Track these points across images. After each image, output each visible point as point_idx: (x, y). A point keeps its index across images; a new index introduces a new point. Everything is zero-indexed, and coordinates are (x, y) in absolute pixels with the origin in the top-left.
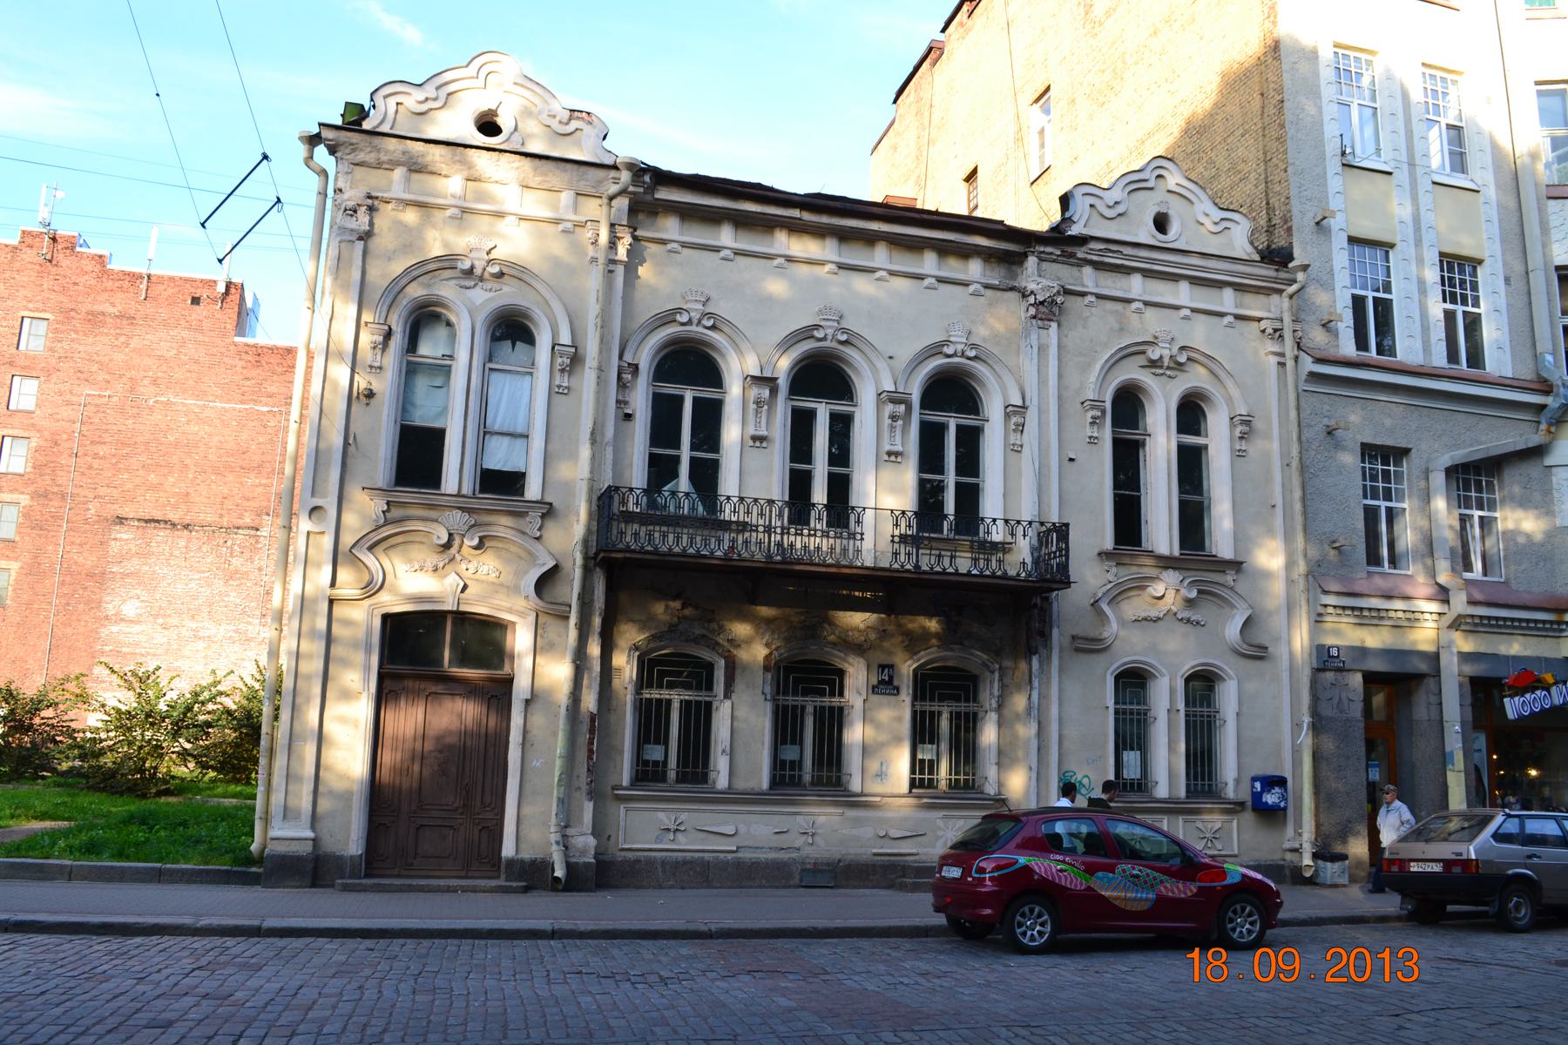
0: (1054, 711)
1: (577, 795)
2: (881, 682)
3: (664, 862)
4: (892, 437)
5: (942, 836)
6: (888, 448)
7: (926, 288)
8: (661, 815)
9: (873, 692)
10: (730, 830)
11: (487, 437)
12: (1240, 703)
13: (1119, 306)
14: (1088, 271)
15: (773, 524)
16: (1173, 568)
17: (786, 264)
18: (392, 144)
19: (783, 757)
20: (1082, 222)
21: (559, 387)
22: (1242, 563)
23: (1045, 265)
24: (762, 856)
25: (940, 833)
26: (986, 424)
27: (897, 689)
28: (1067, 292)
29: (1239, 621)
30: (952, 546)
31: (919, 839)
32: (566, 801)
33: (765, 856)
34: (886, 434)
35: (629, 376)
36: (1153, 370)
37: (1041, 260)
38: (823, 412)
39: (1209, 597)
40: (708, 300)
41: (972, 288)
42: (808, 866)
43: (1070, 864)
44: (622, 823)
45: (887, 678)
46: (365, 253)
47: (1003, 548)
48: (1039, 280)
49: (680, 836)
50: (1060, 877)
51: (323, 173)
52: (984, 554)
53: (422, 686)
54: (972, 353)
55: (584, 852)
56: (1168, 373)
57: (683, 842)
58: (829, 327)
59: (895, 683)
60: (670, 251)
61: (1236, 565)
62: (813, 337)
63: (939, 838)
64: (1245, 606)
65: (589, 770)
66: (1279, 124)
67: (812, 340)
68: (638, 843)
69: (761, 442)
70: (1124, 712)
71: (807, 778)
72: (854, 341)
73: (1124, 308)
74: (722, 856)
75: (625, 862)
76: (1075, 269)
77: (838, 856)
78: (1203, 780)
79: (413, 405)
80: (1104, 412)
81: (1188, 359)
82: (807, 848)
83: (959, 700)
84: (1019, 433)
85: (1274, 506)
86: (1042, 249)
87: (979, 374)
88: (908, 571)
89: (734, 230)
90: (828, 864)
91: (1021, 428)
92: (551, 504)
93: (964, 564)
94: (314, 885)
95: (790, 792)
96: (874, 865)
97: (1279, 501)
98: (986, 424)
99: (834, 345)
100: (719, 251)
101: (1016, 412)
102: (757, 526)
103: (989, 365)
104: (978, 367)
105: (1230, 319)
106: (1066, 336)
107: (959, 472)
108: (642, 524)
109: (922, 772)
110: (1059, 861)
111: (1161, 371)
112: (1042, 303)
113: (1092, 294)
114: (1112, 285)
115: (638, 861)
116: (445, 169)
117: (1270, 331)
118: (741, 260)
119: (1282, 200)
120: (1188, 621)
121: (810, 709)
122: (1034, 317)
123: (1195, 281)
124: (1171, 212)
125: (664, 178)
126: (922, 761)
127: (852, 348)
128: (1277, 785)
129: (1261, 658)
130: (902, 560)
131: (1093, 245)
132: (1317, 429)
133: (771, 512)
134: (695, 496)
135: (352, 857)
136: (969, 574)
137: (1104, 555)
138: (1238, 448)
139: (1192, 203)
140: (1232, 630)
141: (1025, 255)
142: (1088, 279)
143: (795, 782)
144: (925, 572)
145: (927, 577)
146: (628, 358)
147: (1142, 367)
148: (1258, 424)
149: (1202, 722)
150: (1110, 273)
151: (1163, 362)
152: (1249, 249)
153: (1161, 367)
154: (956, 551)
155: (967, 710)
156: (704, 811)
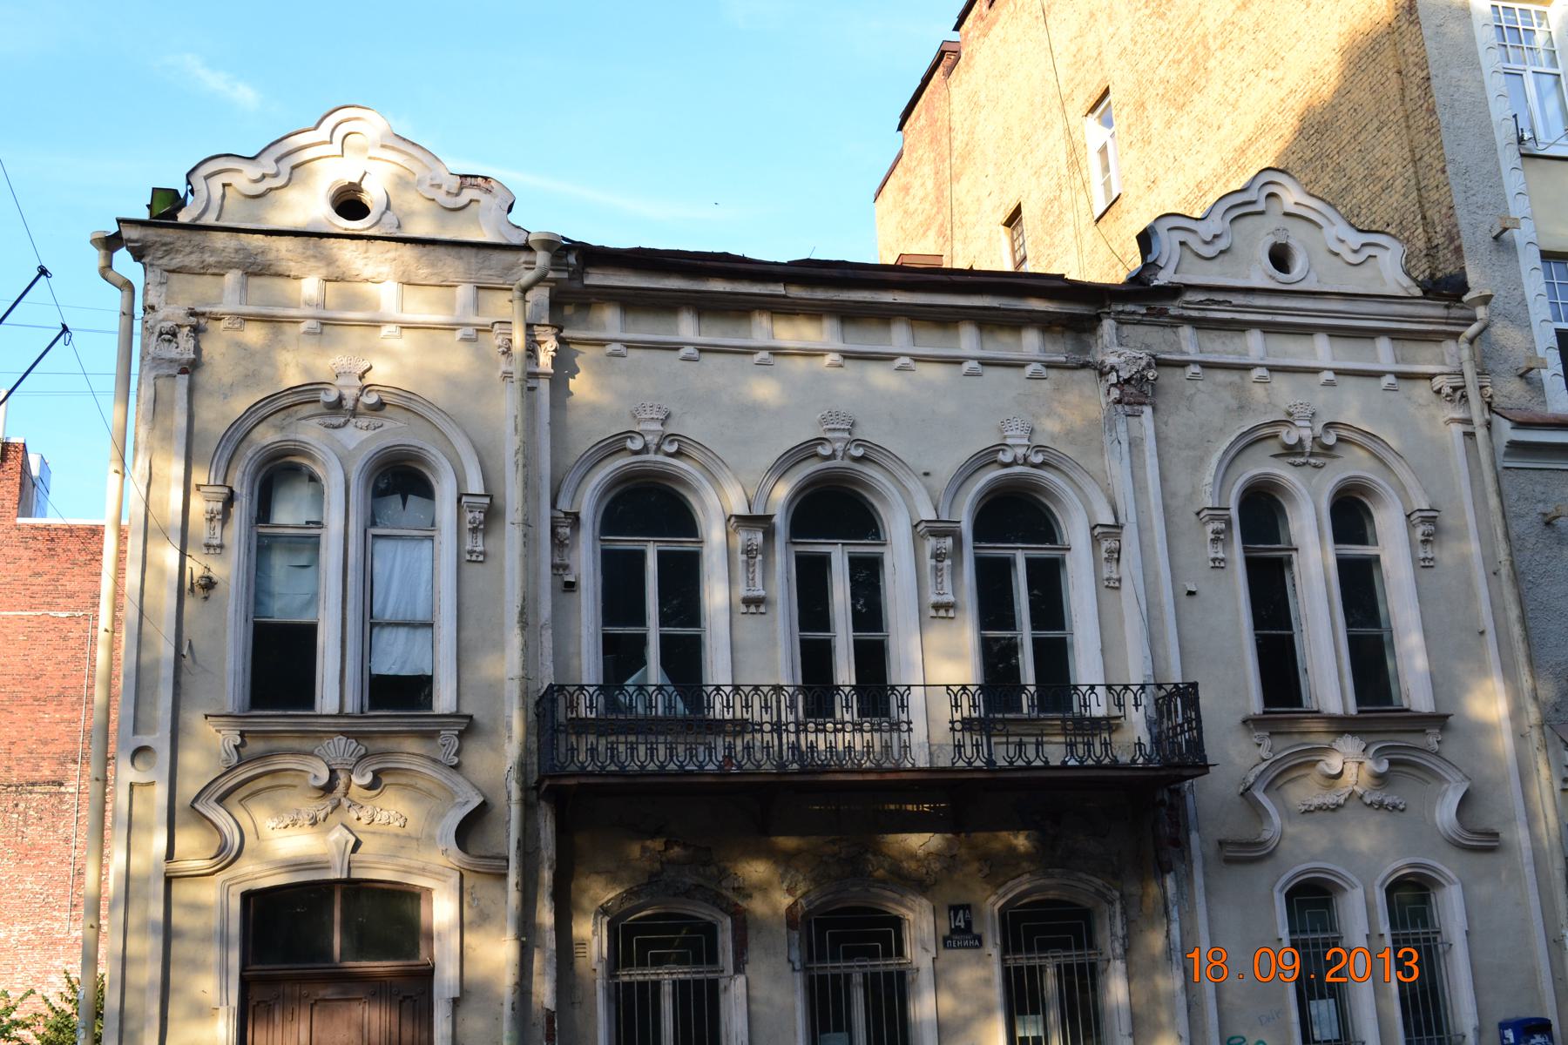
2: (955, 931)
4: (938, 584)
6: (933, 598)
7: (967, 375)
11: (375, 631)
12: (1469, 918)
13: (1234, 377)
14: (1186, 332)
17: (913, 364)
18: (220, 240)
21: (471, 552)
23: (1126, 330)
26: (1294, 554)
27: (979, 938)
28: (1161, 364)
34: (929, 580)
36: (1292, 460)
37: (1120, 323)
38: (839, 557)
40: (668, 416)
45: (962, 925)
46: (191, 391)
47: (1109, 724)
48: (1121, 350)
51: (127, 286)
54: (1038, 459)
56: (1313, 461)
58: (838, 440)
59: (976, 930)
62: (816, 455)
64: (1459, 777)
66: (1427, 109)
67: (995, 465)
69: (757, 607)
72: (874, 456)
76: (1168, 330)
78: (1429, 1032)
80: (1229, 523)
83: (1068, 948)
85: (1482, 633)
86: (1120, 308)
88: (979, 769)
91: (1115, 556)
92: (471, 717)
93: (1055, 752)
97: (1488, 623)
98: (1294, 554)
99: (847, 463)
101: (1106, 535)
102: (761, 724)
103: (1056, 468)
105: (1389, 380)
106: (1166, 424)
108: (600, 734)
111: (1302, 460)
112: (1127, 381)
113: (1195, 362)
114: (1221, 348)
116: (294, 269)
117: (1447, 390)
119: (1444, 211)
122: (1119, 402)
123: (1335, 332)
124: (1292, 242)
130: (662, 759)
131: (1190, 297)
133: (779, 702)
137: (1250, 723)
138: (1422, 555)
139: (1320, 227)
140: (1445, 812)
141: (1098, 319)
142: (1188, 343)
146: (564, 505)
148: (1447, 520)
150: (1217, 333)
152: (1406, 282)
153: (1302, 454)
154: (1042, 735)
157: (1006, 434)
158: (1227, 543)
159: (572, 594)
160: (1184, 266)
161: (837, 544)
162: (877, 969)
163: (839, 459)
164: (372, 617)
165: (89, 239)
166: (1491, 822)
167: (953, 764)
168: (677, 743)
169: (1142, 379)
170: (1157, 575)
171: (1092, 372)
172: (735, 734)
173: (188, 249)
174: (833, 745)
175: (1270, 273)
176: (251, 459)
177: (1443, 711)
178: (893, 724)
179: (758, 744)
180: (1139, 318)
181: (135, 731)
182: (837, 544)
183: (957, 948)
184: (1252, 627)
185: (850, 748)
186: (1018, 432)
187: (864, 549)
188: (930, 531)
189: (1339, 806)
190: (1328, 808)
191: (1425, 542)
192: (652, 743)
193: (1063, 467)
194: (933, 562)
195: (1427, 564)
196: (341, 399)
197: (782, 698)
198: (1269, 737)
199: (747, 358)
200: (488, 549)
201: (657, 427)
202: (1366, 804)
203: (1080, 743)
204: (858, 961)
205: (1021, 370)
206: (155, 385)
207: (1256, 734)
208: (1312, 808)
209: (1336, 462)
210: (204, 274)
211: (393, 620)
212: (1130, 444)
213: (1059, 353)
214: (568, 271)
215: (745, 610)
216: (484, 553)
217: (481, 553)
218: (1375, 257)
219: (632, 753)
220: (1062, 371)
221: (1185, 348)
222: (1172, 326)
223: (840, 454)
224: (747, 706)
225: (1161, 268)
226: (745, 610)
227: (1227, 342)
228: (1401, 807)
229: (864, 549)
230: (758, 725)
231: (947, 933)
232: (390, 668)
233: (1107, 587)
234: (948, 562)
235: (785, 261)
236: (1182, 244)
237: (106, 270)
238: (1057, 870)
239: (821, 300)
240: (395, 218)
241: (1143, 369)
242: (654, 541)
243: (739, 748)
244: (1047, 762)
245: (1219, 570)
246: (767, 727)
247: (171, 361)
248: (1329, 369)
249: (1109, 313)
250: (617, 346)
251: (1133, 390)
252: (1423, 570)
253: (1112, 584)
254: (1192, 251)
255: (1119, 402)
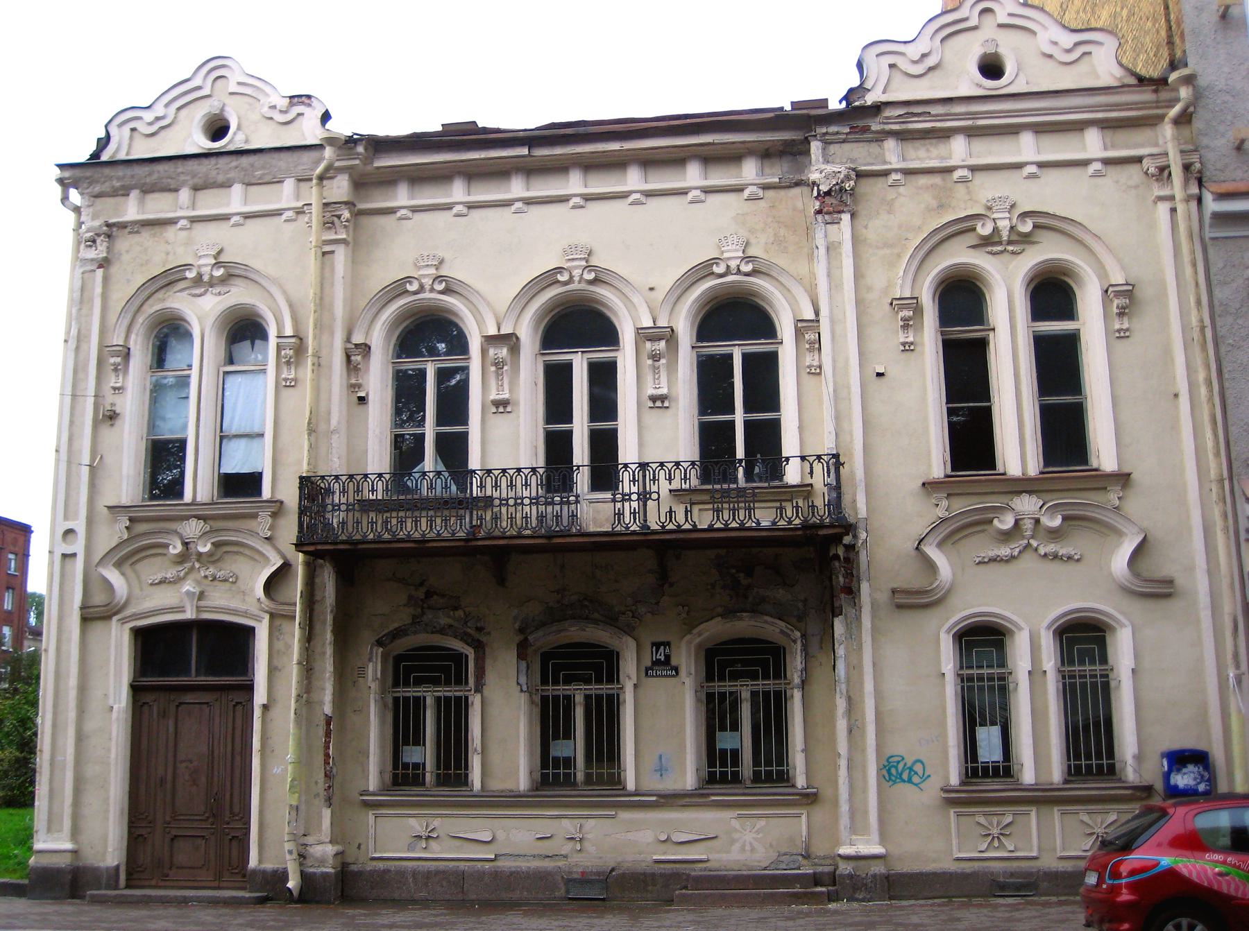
0: (869, 686)
1: (317, 802)
2: (657, 663)
3: (415, 873)
4: (656, 379)
5: (751, 844)
6: (651, 391)
7: (691, 202)
8: (412, 821)
9: (647, 674)
10: (486, 837)
11: (225, 442)
12: (1137, 656)
13: (936, 180)
14: (890, 144)
15: (648, 489)
16: (1026, 492)
17: (525, 208)
19: (406, 759)
20: (880, 87)
21: (286, 380)
22: (1130, 475)
23: (833, 149)
24: (523, 865)
25: (736, 836)
26: (991, 334)
27: (676, 669)
28: (860, 175)
29: (1127, 548)
30: (749, 499)
31: (710, 843)
32: (303, 807)
33: (529, 865)
35: (359, 358)
36: (990, 249)
37: (827, 143)
38: (580, 365)
39: (235, 549)
40: (442, 262)
41: (690, 196)
42: (575, 876)
43: (1234, 866)
44: (372, 831)
45: (663, 658)
46: (106, 280)
47: (805, 490)
48: (823, 167)
49: (433, 844)
50: (1220, 883)
51: (77, 210)
52: (729, 502)
53: (172, 697)
54: (747, 268)
55: (322, 862)
56: (1010, 248)
57: (437, 850)
58: (576, 267)
59: (674, 662)
60: (400, 219)
61: (1123, 479)
62: (558, 282)
63: (733, 841)
64: (1135, 530)
65: (326, 775)
67: (712, 276)
68: (389, 851)
69: (505, 407)
70: (970, 679)
71: (580, 776)
72: (456, 288)
73: (944, 180)
74: (479, 865)
75: (372, 873)
76: (874, 145)
77: (612, 864)
78: (1088, 757)
79: (163, 419)
80: (918, 310)
81: (1035, 227)
82: (575, 855)
83: (756, 678)
84: (816, 353)
85: (1176, 396)
86: (824, 130)
87: (762, 291)
88: (634, 533)
89: (643, 169)
90: (598, 873)
91: (817, 345)
92: (282, 502)
93: (765, 517)
94: (73, 896)
95: (562, 793)
96: (653, 875)
97: (1183, 387)
98: (991, 334)
99: (583, 286)
100: (281, 214)
102: (630, 495)
103: (768, 275)
104: (759, 282)
105: (1097, 166)
106: (866, 227)
107: (440, 420)
108: (379, 511)
109: (724, 765)
110: (1217, 862)
111: (1000, 248)
112: (828, 193)
113: (896, 171)
114: (925, 156)
115: (387, 871)
117: (1152, 170)
118: (476, 214)
120: (1056, 557)
121: (579, 699)
122: (819, 212)
123: (1040, 129)
124: (1001, 50)
125: (379, 145)
126: (724, 752)
127: (604, 285)
128: (1191, 763)
129: (1167, 596)
131: (888, 113)
132: (1234, 285)
133: (644, 476)
134: (446, 474)
135: (107, 868)
136: (711, 529)
137: (929, 486)
138: (1117, 326)
139: (1033, 33)
140: (1119, 560)
141: (807, 141)
142: (892, 154)
143: (569, 781)
144: (655, 532)
145: (657, 537)
146: (358, 338)
147: (973, 247)
148: (1146, 293)
149: (1084, 685)
150: (922, 142)
151: (1000, 237)
152: (1118, 72)
153: (1000, 243)
154: (754, 502)
155: (777, 688)
156: (457, 816)
157: (723, 249)
158: (919, 328)
159: (365, 406)
160: (894, 85)
161: (577, 352)
162: (408, 694)
163: (576, 283)
164: (221, 430)
165: (55, 178)
166: (1168, 569)
167: (613, 529)
168: (436, 517)
169: (841, 190)
170: (847, 360)
171: (806, 188)
172: (485, 508)
173: (103, 179)
174: (514, 516)
175: (976, 81)
176: (142, 324)
177: (1126, 470)
178: (505, 505)
179: (519, 515)
180: (844, 136)
181: (66, 518)
182: (577, 352)
183: (657, 676)
184: (696, 411)
185: (734, 511)
186: (734, 247)
187: (601, 355)
188: (645, 337)
189: (1013, 557)
190: (1002, 560)
191: (1121, 315)
192: (416, 517)
193: (772, 273)
194: (650, 362)
195: (1122, 334)
196: (200, 276)
197: (647, 472)
198: (947, 498)
199: (506, 209)
200: (298, 376)
201: (432, 271)
202: (1040, 555)
203: (726, 509)
204: (424, 687)
205: (740, 193)
206: (83, 278)
207: (935, 495)
208: (986, 560)
209: (1037, 247)
210: (117, 196)
211: (238, 433)
212: (828, 249)
213: (773, 175)
214: (358, 158)
215: (495, 410)
216: (295, 380)
217: (292, 380)
218: (1090, 53)
219: (416, 525)
220: (779, 191)
221: (888, 159)
222: (877, 141)
223: (576, 279)
224: (496, 486)
225: (869, 90)
226: (495, 410)
227: (932, 149)
228: (1076, 557)
229: (601, 355)
230: (505, 500)
231: (649, 664)
232: (233, 469)
233: (809, 373)
234: (663, 361)
235: (533, 127)
236: (892, 66)
237: (65, 199)
238: (744, 614)
239: (560, 155)
240: (244, 136)
241: (842, 182)
242: (432, 361)
243: (488, 518)
244: (695, 526)
245: (908, 354)
246: (527, 501)
247: (92, 260)
248: (696, 188)
249: (815, 136)
250: (637, 196)
251: (834, 201)
252: (1118, 341)
253: (813, 371)
254: (901, 70)
255: (819, 212)
